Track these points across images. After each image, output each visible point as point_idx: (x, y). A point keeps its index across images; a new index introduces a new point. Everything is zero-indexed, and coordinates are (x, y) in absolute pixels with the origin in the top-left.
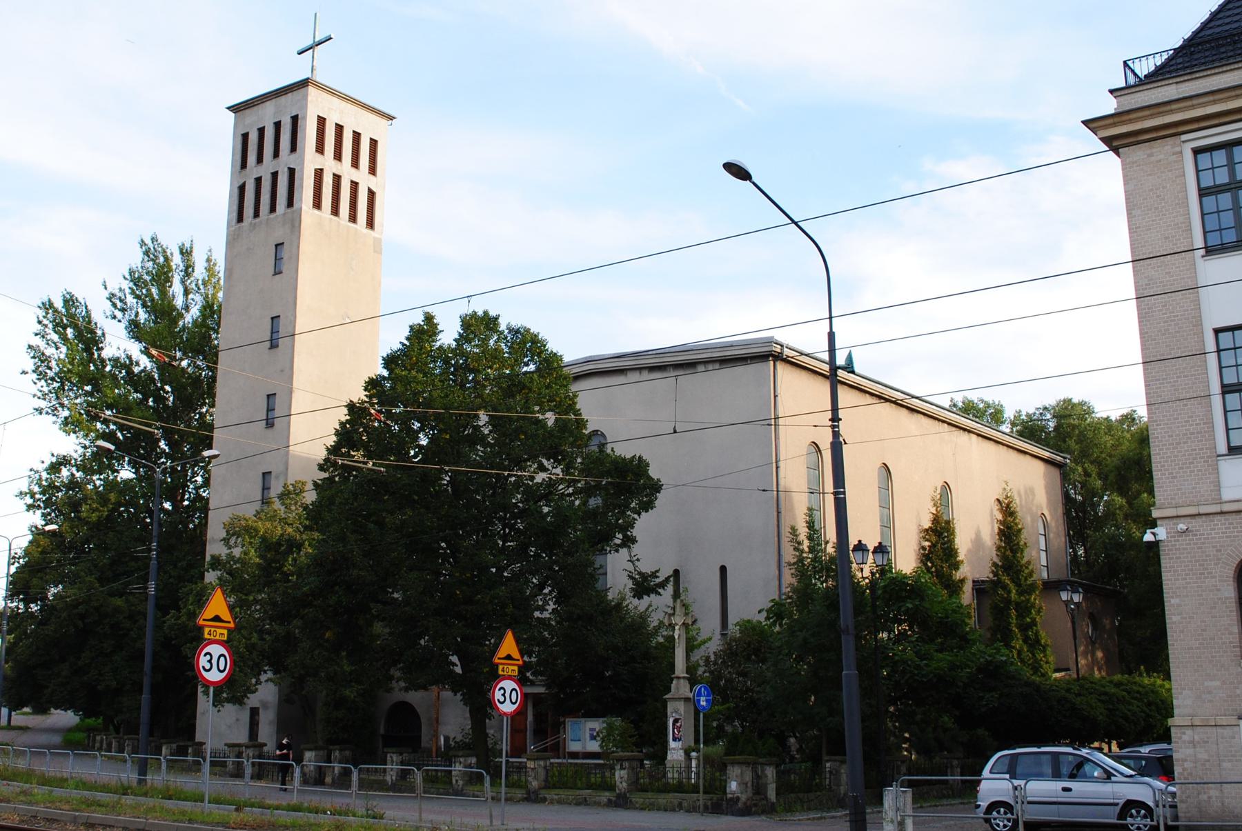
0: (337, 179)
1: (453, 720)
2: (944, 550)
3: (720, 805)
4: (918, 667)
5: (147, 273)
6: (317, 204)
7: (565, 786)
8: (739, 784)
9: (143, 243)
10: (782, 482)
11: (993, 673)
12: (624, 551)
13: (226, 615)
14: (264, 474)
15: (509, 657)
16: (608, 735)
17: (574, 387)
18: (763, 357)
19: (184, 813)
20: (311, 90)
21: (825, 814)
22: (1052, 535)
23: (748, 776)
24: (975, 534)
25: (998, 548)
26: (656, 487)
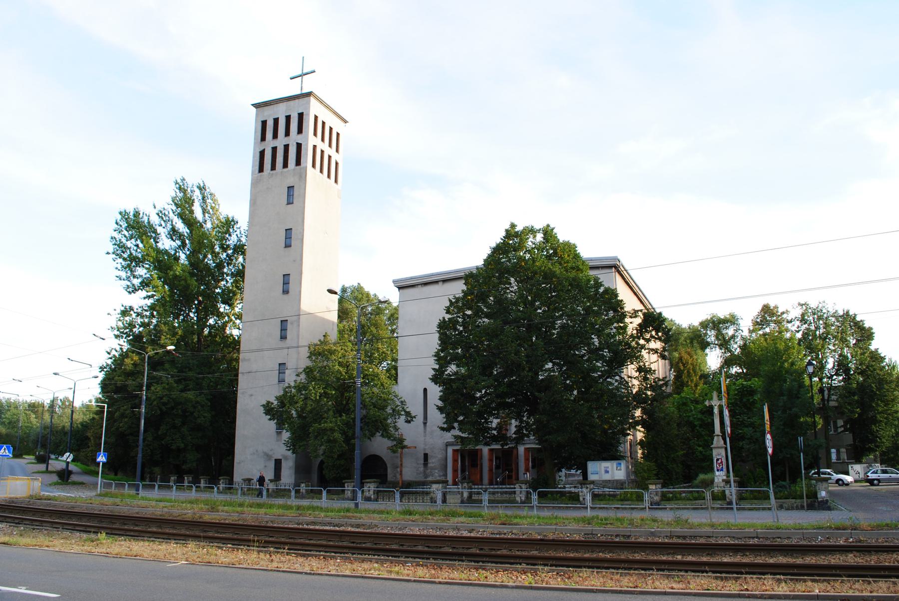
9: (177, 183)
20: (312, 98)
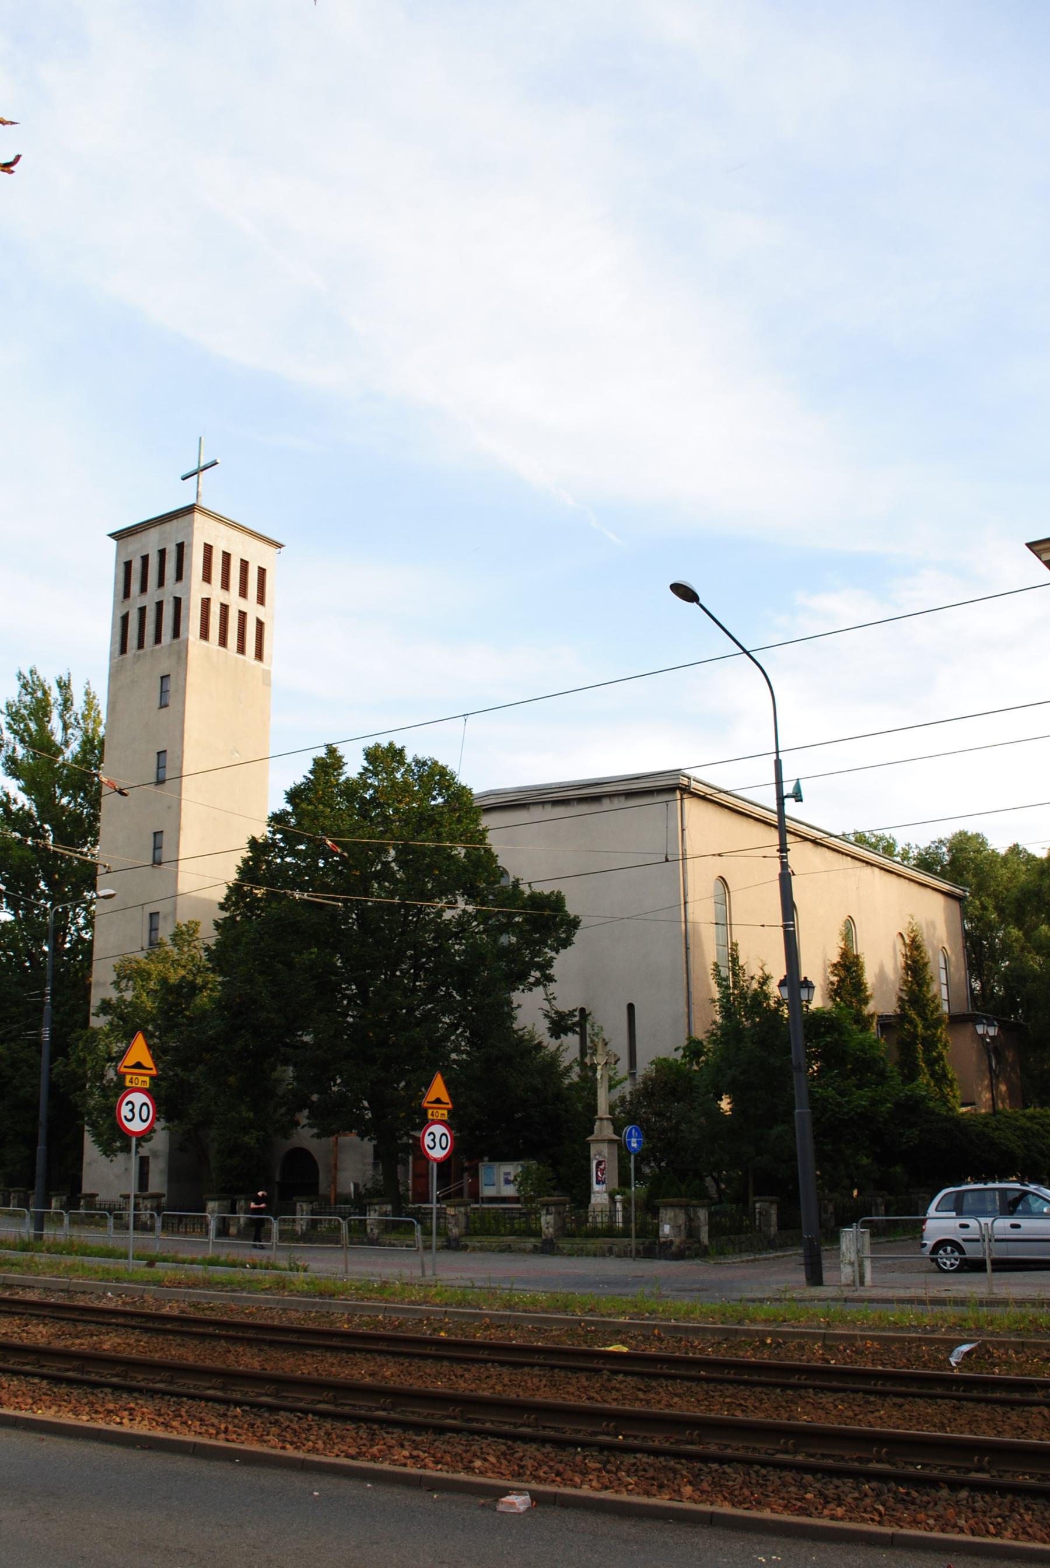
0: (225, 608)
1: (353, 1162)
2: (854, 984)
3: (653, 1249)
4: (839, 1105)
5: (25, 707)
6: (205, 635)
7: (487, 1232)
8: (672, 1227)
9: (20, 676)
10: (690, 918)
11: (912, 1109)
12: (539, 990)
13: (148, 1061)
14: (151, 915)
15: (438, 1101)
16: (527, 1179)
17: (486, 821)
18: (671, 790)
19: (108, 1271)
20: (197, 516)
21: (757, 1256)
22: (952, 969)
23: (682, 1219)
24: (881, 965)
25: (906, 982)
26: (574, 924)
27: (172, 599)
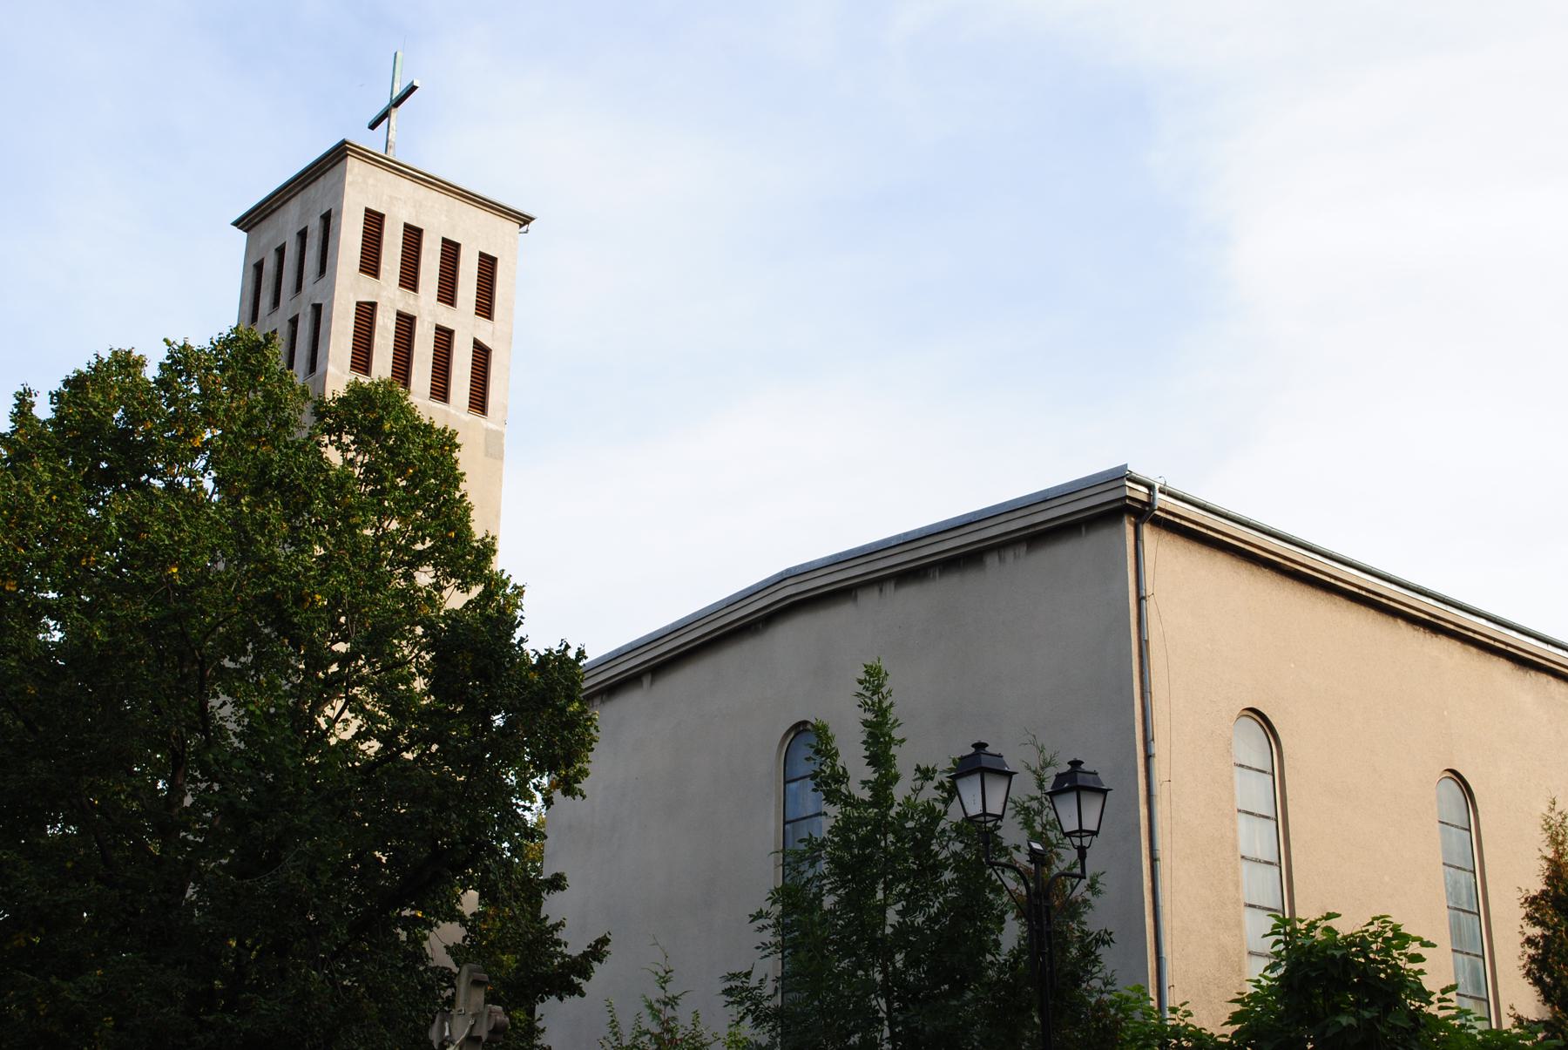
27: (309, 309)
